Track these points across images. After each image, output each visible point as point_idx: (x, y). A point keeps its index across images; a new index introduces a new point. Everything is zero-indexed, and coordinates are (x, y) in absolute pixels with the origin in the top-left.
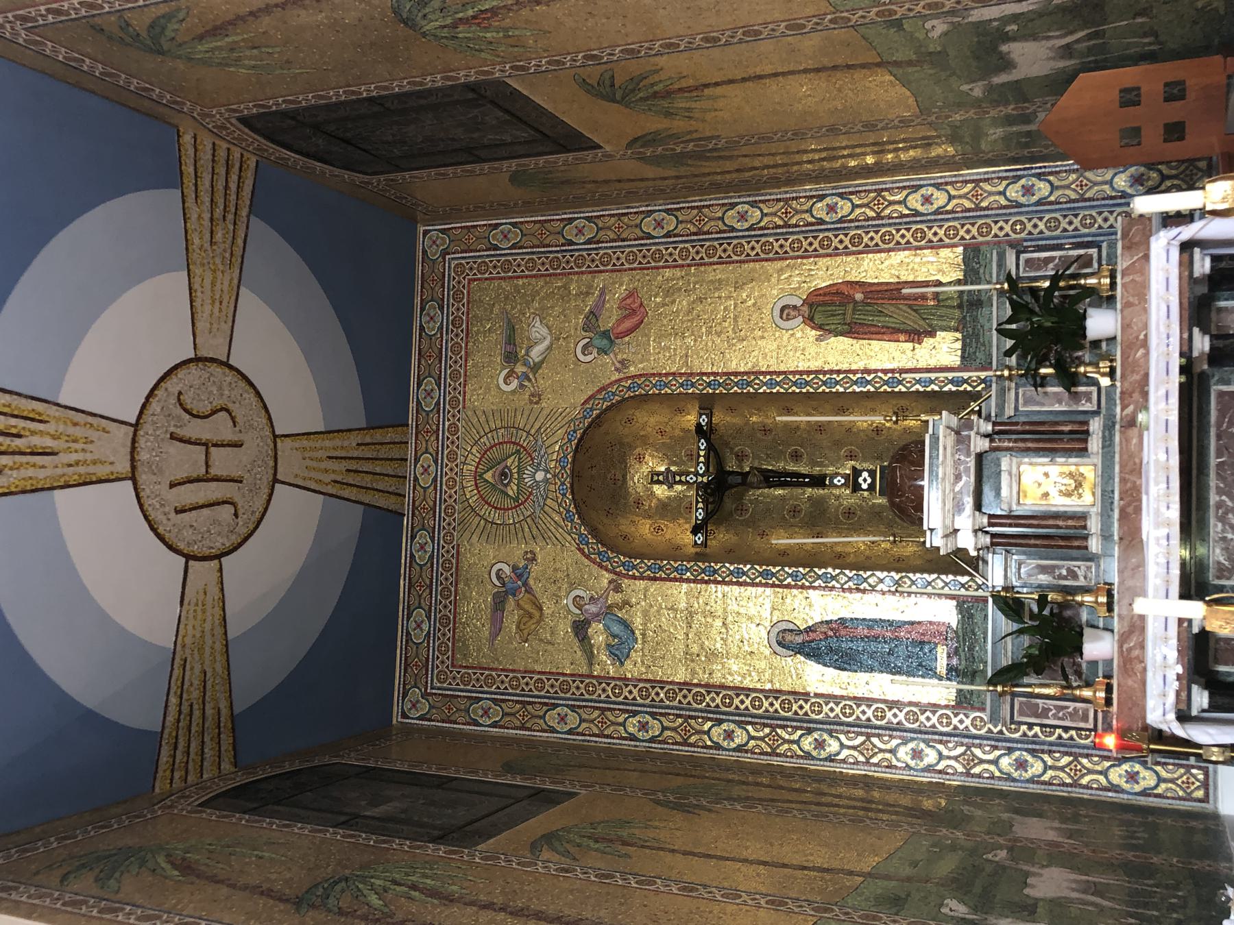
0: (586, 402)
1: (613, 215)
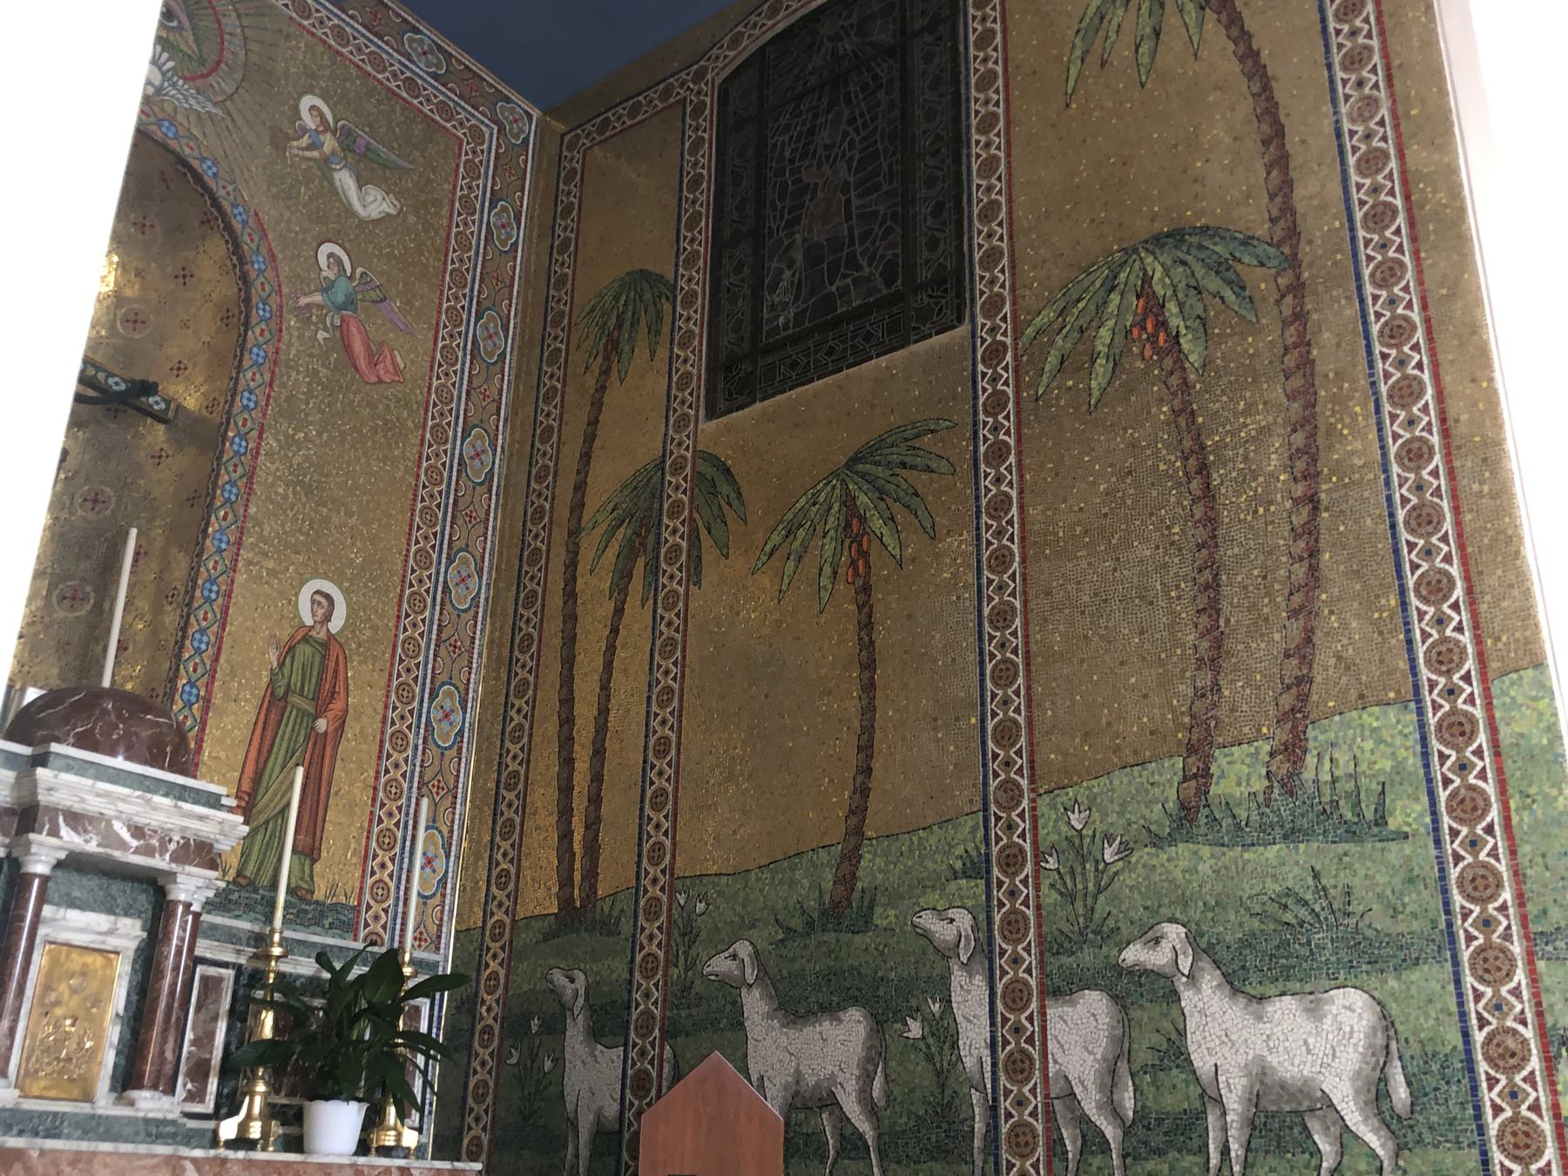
1: (500, 394)
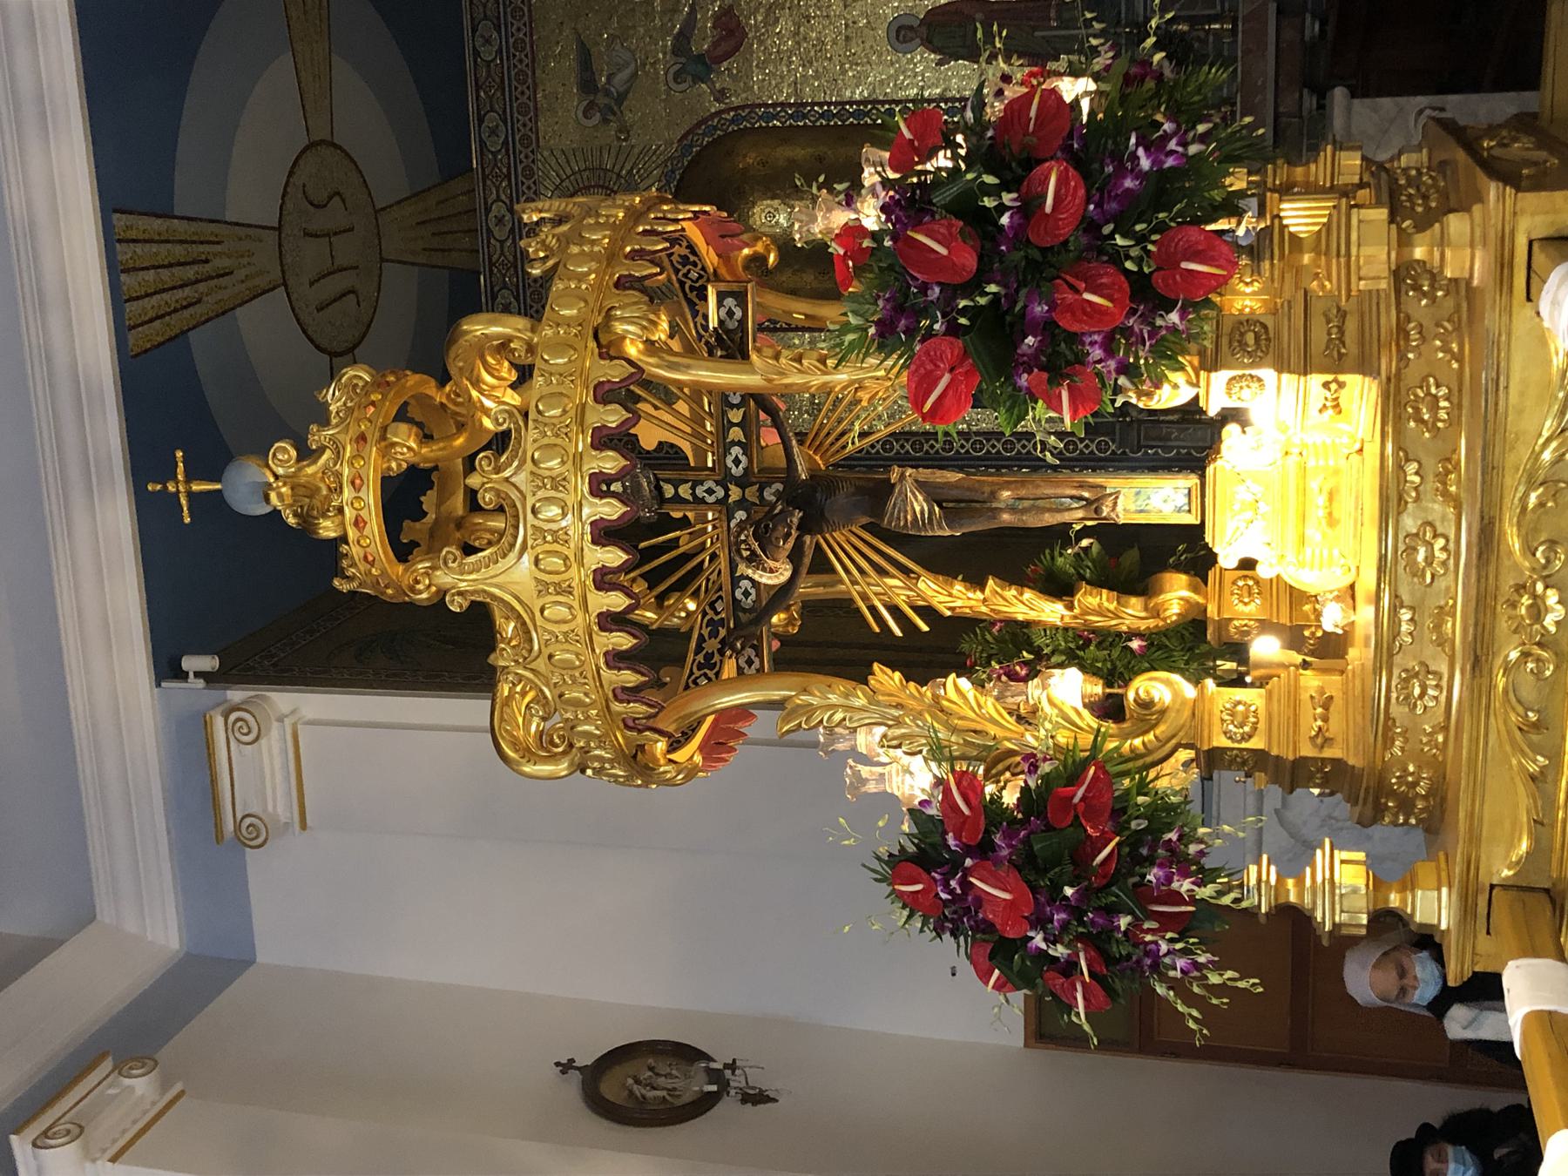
0: (684, 137)
